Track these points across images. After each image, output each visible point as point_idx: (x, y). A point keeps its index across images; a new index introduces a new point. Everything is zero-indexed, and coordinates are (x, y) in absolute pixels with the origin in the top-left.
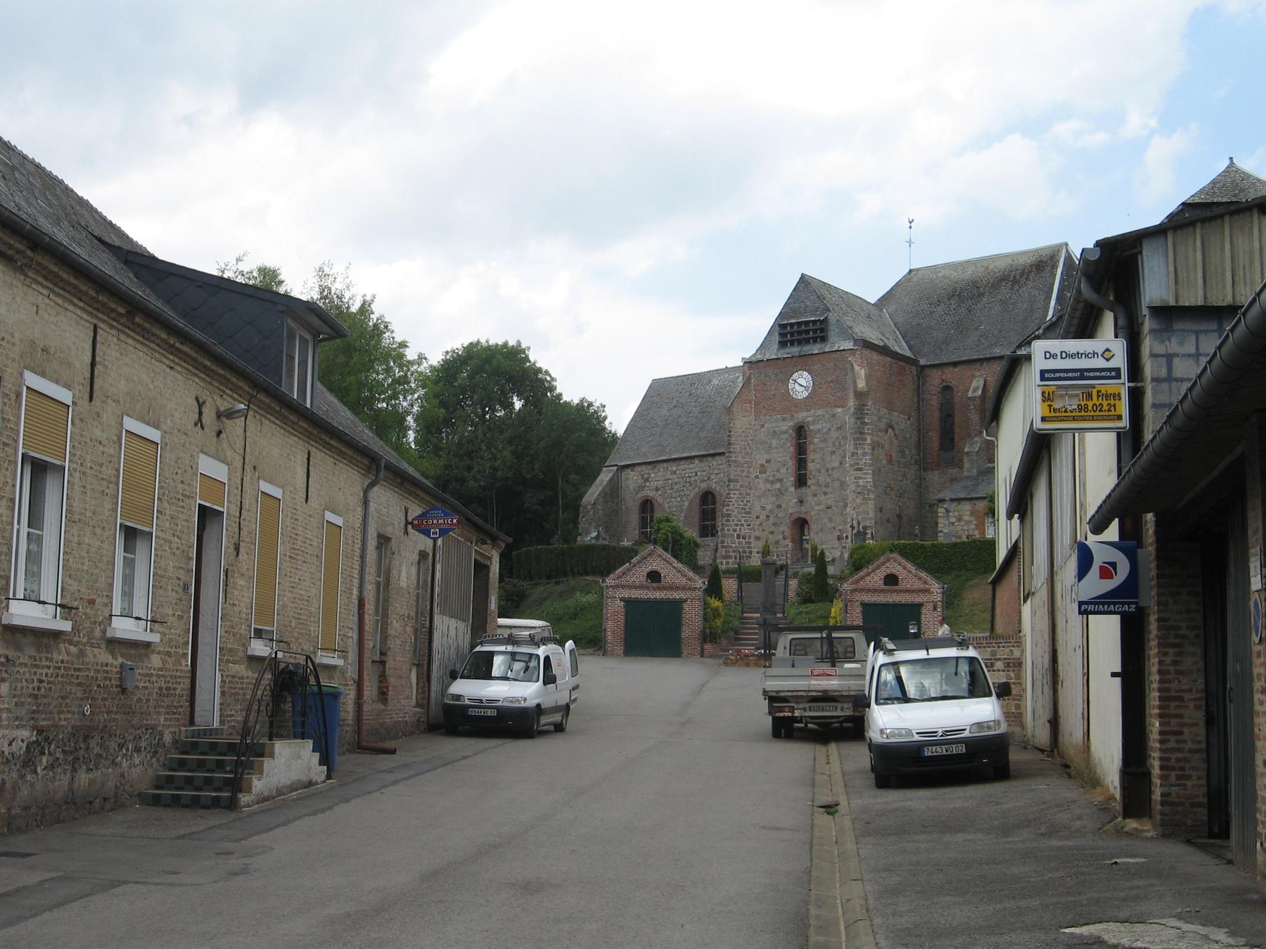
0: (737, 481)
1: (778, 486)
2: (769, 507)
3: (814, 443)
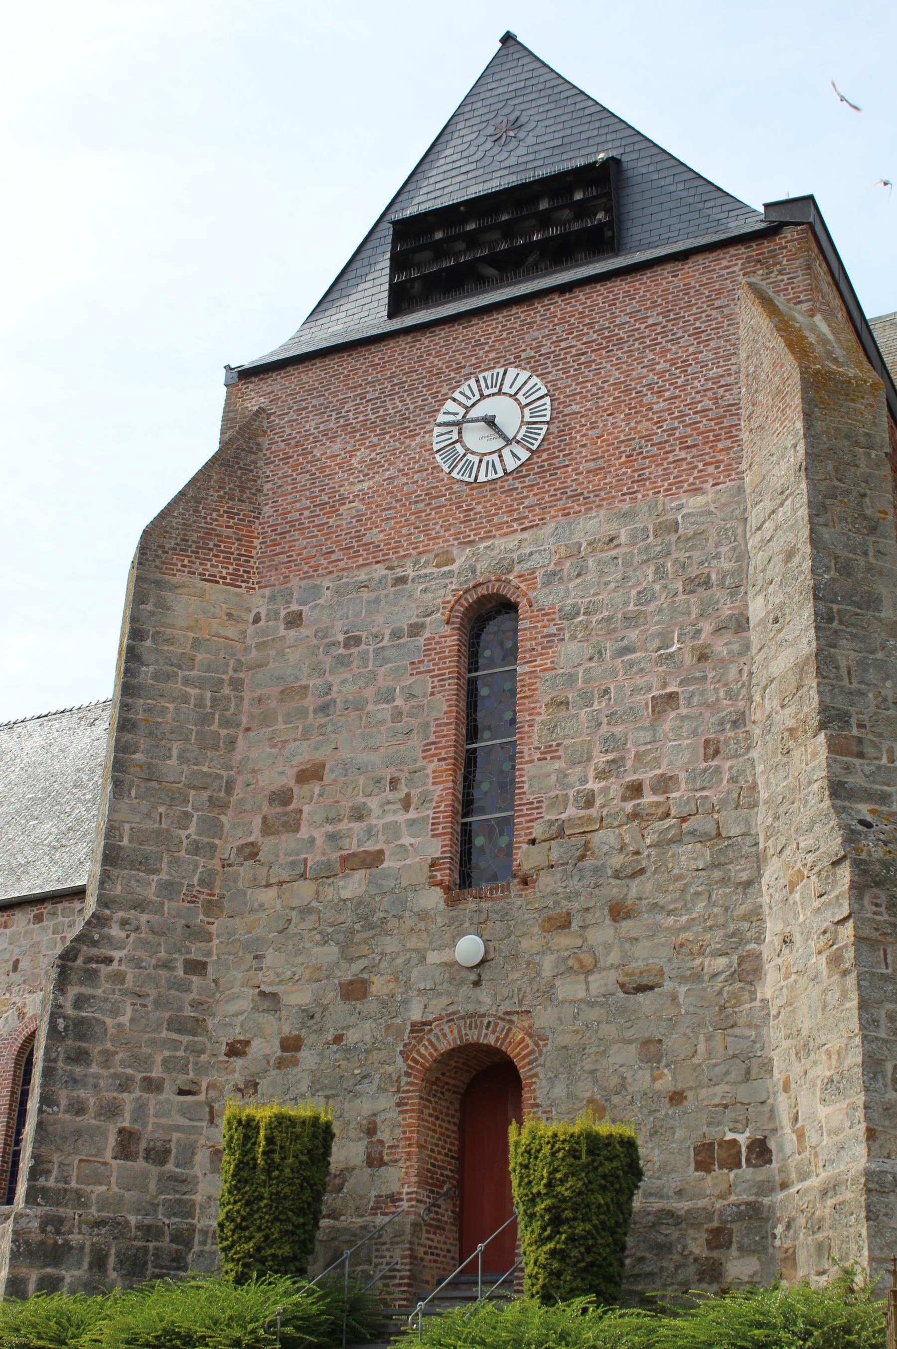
0: (146, 864)
2: (298, 997)
3: (549, 665)
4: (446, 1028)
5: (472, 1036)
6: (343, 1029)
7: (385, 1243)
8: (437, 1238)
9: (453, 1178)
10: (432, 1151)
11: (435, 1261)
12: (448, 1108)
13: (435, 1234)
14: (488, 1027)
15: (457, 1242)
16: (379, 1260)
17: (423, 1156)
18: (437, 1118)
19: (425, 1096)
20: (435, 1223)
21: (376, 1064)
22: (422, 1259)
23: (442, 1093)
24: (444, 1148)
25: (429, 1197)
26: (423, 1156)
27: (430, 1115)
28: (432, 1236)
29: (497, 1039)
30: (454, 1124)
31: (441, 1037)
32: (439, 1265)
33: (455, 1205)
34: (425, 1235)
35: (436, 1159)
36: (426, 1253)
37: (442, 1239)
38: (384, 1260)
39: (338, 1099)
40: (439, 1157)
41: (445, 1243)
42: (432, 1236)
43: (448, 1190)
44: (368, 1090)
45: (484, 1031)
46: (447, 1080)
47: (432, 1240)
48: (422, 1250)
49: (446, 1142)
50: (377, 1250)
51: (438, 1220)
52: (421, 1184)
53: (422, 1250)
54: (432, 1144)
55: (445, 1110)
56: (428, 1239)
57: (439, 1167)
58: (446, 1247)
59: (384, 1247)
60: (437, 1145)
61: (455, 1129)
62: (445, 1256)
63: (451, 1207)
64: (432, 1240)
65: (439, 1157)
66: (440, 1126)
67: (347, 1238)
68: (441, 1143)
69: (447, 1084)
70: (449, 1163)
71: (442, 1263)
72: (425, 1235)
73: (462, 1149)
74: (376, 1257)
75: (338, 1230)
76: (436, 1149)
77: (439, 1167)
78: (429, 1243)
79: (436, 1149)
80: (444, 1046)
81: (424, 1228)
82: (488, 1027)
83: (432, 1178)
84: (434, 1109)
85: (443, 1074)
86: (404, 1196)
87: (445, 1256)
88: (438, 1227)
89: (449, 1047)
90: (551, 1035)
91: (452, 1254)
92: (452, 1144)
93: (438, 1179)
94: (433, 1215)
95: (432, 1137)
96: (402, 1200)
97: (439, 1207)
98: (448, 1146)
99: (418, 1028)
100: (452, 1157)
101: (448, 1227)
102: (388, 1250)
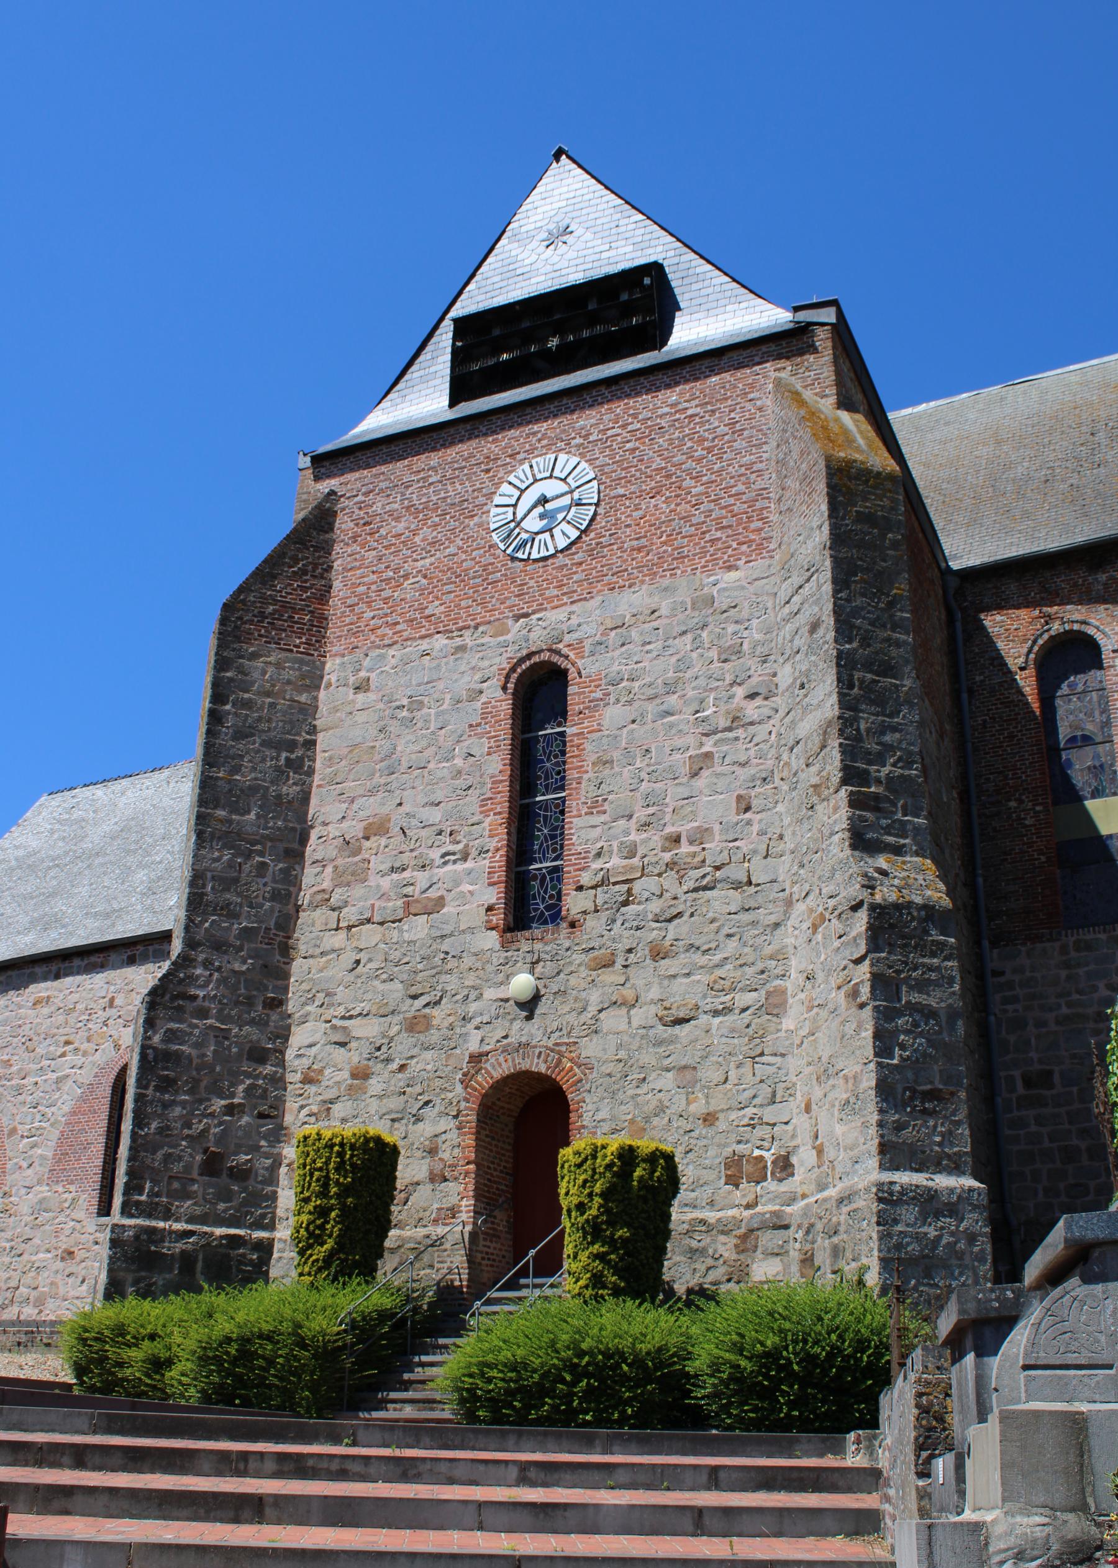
1: (418, 928)
4: (501, 1059)
6: (408, 1059)
7: (445, 1250)
8: (493, 1245)
11: (492, 1266)
13: (491, 1241)
14: (539, 1057)
16: (441, 1265)
24: (499, 1165)
25: (485, 1209)
28: (488, 1243)
29: (548, 1068)
33: (509, 1216)
34: (482, 1243)
35: (492, 1175)
38: (446, 1265)
40: (495, 1173)
42: (488, 1243)
43: (503, 1202)
45: (536, 1060)
46: (502, 1104)
48: (479, 1255)
49: (501, 1160)
51: (494, 1229)
52: (478, 1197)
53: (479, 1255)
56: (485, 1246)
57: (495, 1182)
59: (445, 1254)
60: (493, 1163)
65: (495, 1173)
66: (496, 1146)
67: (412, 1245)
69: (503, 1108)
70: (504, 1179)
72: (482, 1243)
75: (403, 1239)
77: (495, 1182)
80: (497, 1074)
82: (539, 1057)
83: (488, 1192)
85: (499, 1099)
87: (500, 1261)
88: (494, 1236)
92: (506, 1162)
93: (494, 1193)
94: (489, 1225)
97: (495, 1217)
99: (476, 1059)
100: (507, 1174)
102: (449, 1256)
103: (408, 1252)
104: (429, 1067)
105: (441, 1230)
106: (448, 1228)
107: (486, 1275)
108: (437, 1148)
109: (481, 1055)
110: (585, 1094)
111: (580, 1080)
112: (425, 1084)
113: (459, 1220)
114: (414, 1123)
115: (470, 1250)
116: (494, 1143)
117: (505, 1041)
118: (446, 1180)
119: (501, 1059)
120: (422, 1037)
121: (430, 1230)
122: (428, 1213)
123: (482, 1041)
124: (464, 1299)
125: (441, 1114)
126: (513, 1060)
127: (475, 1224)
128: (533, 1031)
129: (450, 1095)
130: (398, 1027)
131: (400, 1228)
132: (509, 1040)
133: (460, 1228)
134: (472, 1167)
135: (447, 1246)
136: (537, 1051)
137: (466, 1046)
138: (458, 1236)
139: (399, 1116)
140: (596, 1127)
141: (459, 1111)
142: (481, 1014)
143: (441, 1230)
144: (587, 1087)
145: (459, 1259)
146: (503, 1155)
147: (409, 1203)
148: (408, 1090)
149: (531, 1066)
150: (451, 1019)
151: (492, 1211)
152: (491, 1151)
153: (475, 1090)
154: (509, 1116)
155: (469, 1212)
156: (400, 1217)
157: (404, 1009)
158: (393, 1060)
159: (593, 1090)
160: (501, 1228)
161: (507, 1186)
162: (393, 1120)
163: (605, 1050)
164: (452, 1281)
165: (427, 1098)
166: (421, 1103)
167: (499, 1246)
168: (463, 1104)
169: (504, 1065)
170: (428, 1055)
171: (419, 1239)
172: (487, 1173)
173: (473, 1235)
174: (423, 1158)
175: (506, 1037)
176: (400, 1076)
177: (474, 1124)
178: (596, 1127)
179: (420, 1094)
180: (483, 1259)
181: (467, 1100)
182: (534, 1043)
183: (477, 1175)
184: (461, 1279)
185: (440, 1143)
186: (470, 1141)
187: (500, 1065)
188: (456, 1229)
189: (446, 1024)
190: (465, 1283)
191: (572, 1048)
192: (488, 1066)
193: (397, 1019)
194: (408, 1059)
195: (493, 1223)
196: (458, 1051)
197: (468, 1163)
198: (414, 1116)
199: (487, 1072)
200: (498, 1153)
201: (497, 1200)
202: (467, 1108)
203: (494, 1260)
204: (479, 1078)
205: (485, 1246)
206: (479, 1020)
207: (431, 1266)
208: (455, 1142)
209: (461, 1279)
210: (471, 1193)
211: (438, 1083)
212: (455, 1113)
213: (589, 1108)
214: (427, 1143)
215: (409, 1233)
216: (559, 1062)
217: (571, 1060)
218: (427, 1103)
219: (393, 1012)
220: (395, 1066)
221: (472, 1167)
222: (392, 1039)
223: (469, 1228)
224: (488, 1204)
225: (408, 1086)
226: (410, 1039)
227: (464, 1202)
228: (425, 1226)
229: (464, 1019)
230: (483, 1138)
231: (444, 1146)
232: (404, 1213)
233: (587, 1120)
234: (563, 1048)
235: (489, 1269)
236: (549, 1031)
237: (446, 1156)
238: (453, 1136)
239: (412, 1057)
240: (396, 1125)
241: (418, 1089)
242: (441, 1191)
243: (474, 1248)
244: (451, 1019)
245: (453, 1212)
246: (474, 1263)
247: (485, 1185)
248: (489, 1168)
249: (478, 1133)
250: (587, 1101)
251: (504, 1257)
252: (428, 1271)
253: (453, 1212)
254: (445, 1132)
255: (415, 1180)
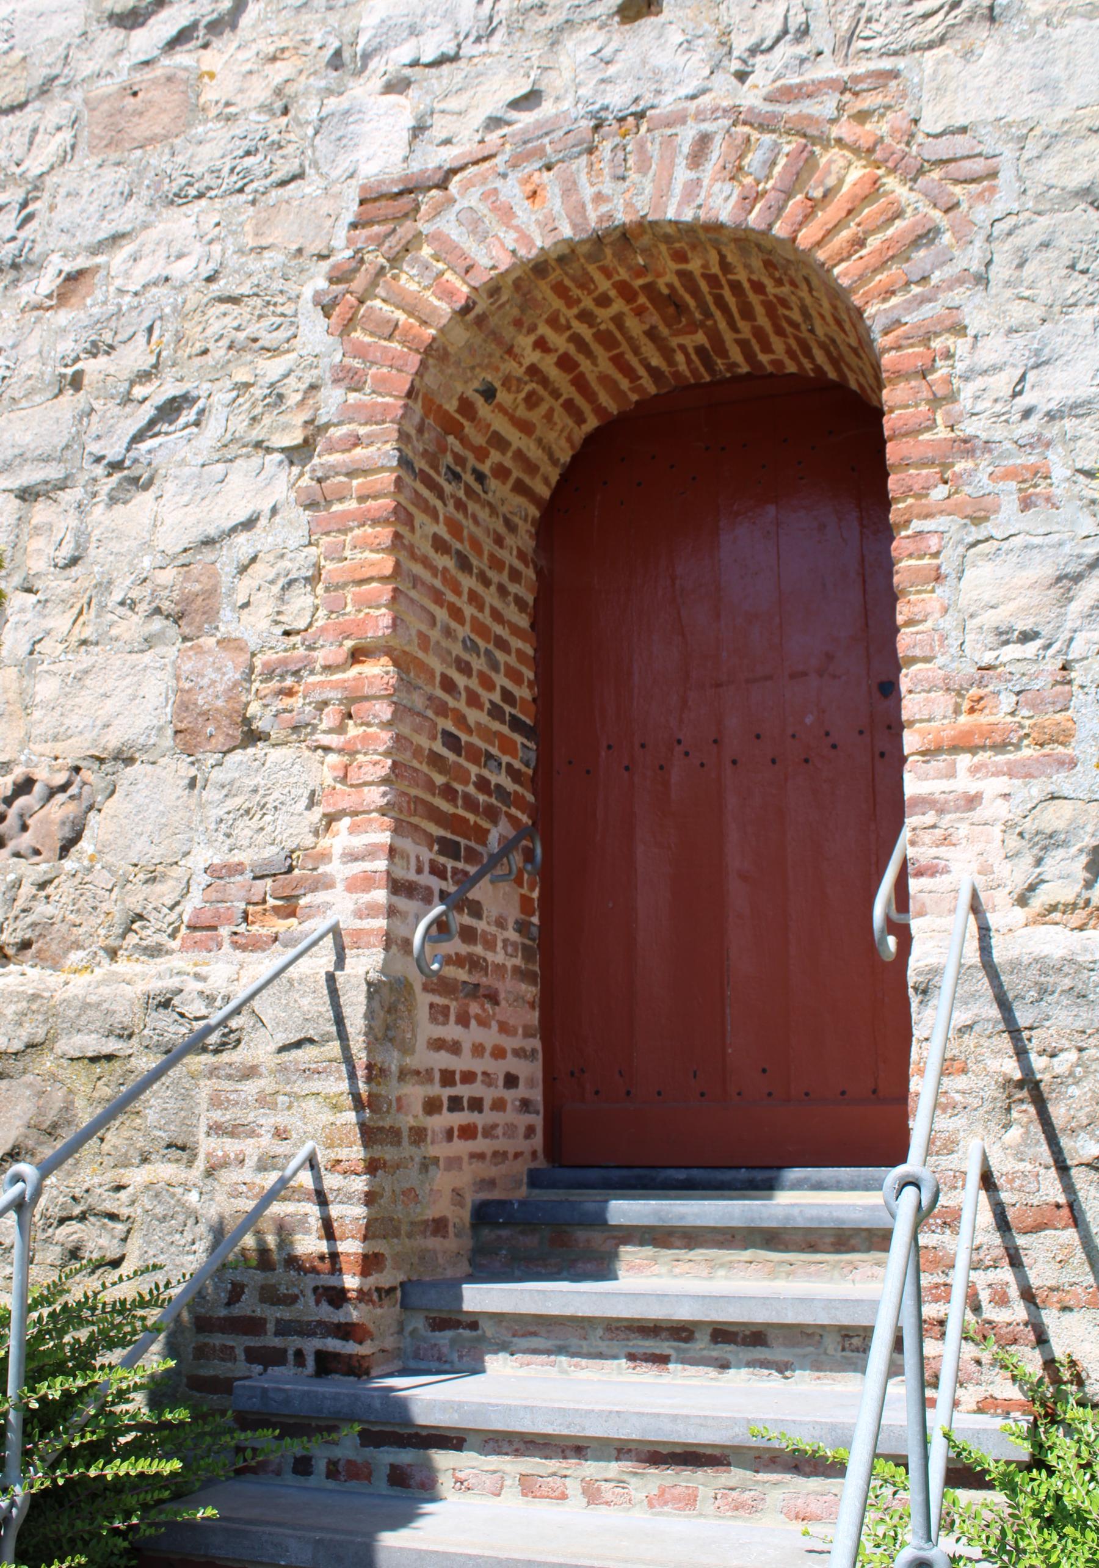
4: (511, 190)
5: (628, 200)
6: (96, 249)
7: (250, 1072)
8: (474, 1034)
9: (517, 801)
10: (448, 685)
11: (468, 1132)
12: (499, 541)
13: (463, 1020)
14: (697, 157)
15: (536, 1043)
16: (231, 1146)
17: (418, 701)
18: (464, 564)
19: (421, 464)
20: (462, 975)
21: (219, 353)
22: (419, 1135)
23: (480, 477)
24: (488, 684)
25: (438, 871)
26: (418, 701)
27: (440, 545)
28: (451, 1031)
29: (749, 200)
30: (520, 602)
31: (491, 221)
32: (481, 1144)
33: (525, 903)
34: (427, 1030)
35: (461, 720)
36: (432, 1106)
37: (490, 1037)
38: (251, 1148)
39: (66, 496)
40: (474, 716)
41: (499, 1053)
42: (451, 1031)
43: (508, 846)
44: (184, 451)
45: (682, 174)
46: (501, 425)
47: (455, 1048)
48: (416, 1093)
49: (494, 666)
50: (216, 1102)
51: (474, 963)
52: (404, 815)
53: (416, 1093)
54: (444, 655)
55: (488, 545)
56: (438, 1044)
57: (475, 755)
58: (499, 1068)
59: (251, 1088)
60: (465, 668)
61: (523, 621)
62: (499, 1105)
63: (513, 914)
64: (455, 1048)
65: (474, 716)
66: (474, 598)
67: (93, 1044)
68: (478, 664)
69: (499, 442)
70: (507, 747)
71: (489, 1132)
72: (427, 1030)
73: (544, 700)
74: (216, 1129)
75: (51, 1014)
76: (461, 680)
77: (475, 755)
78: (443, 1060)
79: (461, 680)
80: (494, 253)
81: (424, 1000)
82: (697, 157)
83: (448, 792)
84: (455, 528)
85: (489, 393)
86: (335, 868)
87: (499, 1105)
88: (474, 991)
89: (527, 253)
90: (1008, 152)
91: (522, 1092)
92: (515, 676)
93: (470, 804)
94: (455, 946)
95: (448, 633)
96: (326, 884)
97: (476, 910)
98: (501, 680)
99: (393, 205)
100: (516, 724)
101: (507, 987)
102: (265, 1101)
103: (68, 1072)
104: (181, 270)
105: (228, 972)
106: (263, 965)
107: (443, 1180)
108: (211, 593)
109: (411, 189)
110: (957, 296)
111: (927, 236)
112: (165, 334)
113: (319, 925)
114: (113, 500)
115: (375, 1072)
116: (468, 582)
117: (525, 119)
118: (252, 737)
119: (511, 190)
120: (157, 158)
121: (172, 971)
122: (166, 892)
123: (418, 130)
124: (346, 1331)
125: (228, 451)
126: (570, 189)
127: (395, 943)
128: (662, 59)
129: (273, 368)
130: (66, 136)
131: (41, 959)
132: (547, 109)
133: (322, 960)
134: (377, 671)
135: (258, 1049)
136: (687, 134)
137: (344, 164)
138: (319, 1005)
139: (53, 472)
140: (1041, 442)
141: (315, 431)
142: (414, 31)
143: (228, 972)
144: (971, 258)
145: (319, 1120)
146: (502, 645)
147: (86, 845)
148: (92, 367)
149: (662, 194)
150: (280, 71)
151: (466, 881)
152: (456, 613)
153: (392, 331)
154: (520, 488)
155: (365, 882)
156: (42, 910)
157: (88, 68)
158: (37, 265)
159: (999, 272)
160: (498, 957)
161: (514, 774)
162: (27, 495)
163: (1048, 86)
164: (284, 1230)
165: (170, 389)
166: (147, 412)
167: (490, 1037)
168: (332, 399)
169: (526, 215)
170: (180, 224)
171: (122, 1016)
172: (442, 710)
173: (388, 998)
174: (149, 642)
175: (530, 99)
176: (63, 317)
177: (386, 480)
178: (1041, 442)
179: (144, 376)
180: (432, 1106)
181: (350, 379)
182: (667, 104)
183: (401, 711)
184: (332, 1221)
185: (226, 569)
186: (369, 553)
187: (506, 213)
188: (304, 966)
189: (260, 91)
190: (350, 1247)
191: (868, 102)
192: (449, 226)
193: (56, 111)
194: (96, 249)
195: (468, 935)
196: (310, 187)
197: (357, 655)
198: (116, 466)
199: (446, 250)
200: (481, 629)
201: (481, 835)
202: (348, 413)
203: (476, 1104)
204: (409, 281)
205: (438, 1044)
206: (403, 54)
207: (181, 1149)
208: (299, 564)
209: (332, 1221)
210: (375, 796)
211: (221, 321)
212: (295, 438)
213: (986, 356)
214: (167, 576)
215: (79, 985)
216: (804, 167)
217: (866, 152)
218: (170, 409)
219: (44, 90)
220: (46, 283)
221: (377, 671)
222: (37, 185)
223: (365, 964)
224: (449, 849)
225: (94, 351)
226: (109, 174)
227: (342, 838)
228: (155, 951)
229: (336, 61)
230: (426, 548)
231: (244, 587)
232: (63, 891)
233: (979, 406)
234: (825, 106)
235: (461, 1147)
236: (741, 43)
237: (254, 627)
238: (288, 537)
239: (116, 239)
240: (41, 512)
241: (135, 356)
242: (229, 789)
243: (393, 1060)
244: (280, 71)
245: (286, 885)
246: (394, 1135)
247: (435, 760)
248: (448, 685)
249: (402, 516)
250: (975, 322)
251: (511, 1081)
252: (164, 1171)
253: (286, 885)
254: (249, 524)
255: (113, 740)
